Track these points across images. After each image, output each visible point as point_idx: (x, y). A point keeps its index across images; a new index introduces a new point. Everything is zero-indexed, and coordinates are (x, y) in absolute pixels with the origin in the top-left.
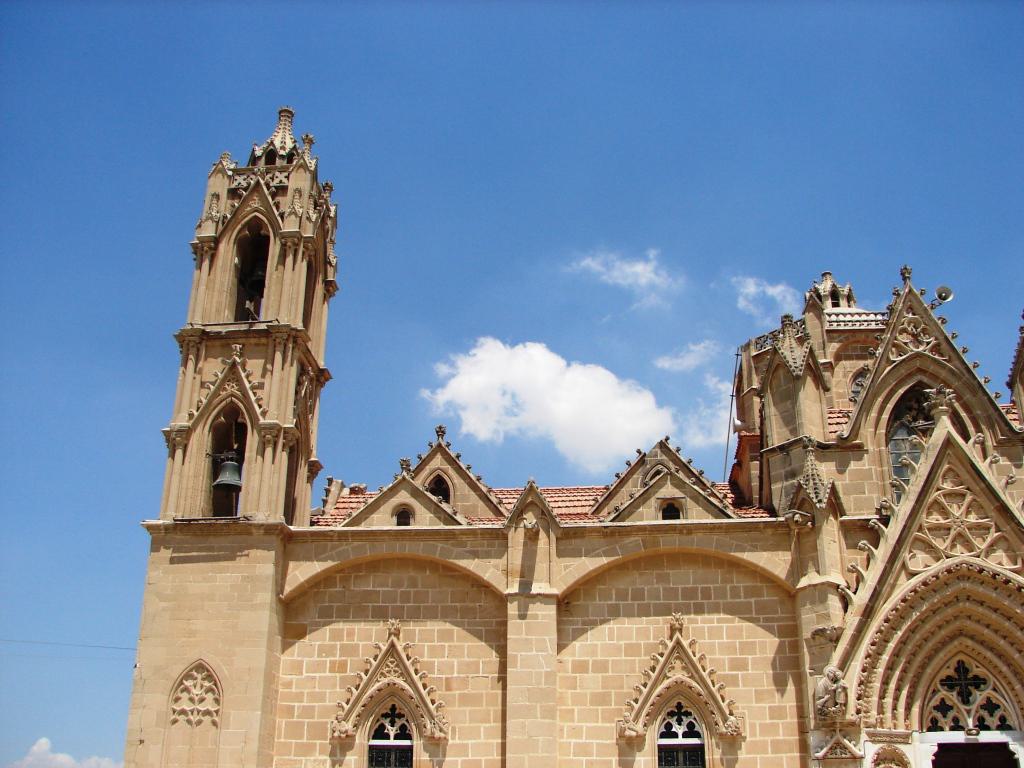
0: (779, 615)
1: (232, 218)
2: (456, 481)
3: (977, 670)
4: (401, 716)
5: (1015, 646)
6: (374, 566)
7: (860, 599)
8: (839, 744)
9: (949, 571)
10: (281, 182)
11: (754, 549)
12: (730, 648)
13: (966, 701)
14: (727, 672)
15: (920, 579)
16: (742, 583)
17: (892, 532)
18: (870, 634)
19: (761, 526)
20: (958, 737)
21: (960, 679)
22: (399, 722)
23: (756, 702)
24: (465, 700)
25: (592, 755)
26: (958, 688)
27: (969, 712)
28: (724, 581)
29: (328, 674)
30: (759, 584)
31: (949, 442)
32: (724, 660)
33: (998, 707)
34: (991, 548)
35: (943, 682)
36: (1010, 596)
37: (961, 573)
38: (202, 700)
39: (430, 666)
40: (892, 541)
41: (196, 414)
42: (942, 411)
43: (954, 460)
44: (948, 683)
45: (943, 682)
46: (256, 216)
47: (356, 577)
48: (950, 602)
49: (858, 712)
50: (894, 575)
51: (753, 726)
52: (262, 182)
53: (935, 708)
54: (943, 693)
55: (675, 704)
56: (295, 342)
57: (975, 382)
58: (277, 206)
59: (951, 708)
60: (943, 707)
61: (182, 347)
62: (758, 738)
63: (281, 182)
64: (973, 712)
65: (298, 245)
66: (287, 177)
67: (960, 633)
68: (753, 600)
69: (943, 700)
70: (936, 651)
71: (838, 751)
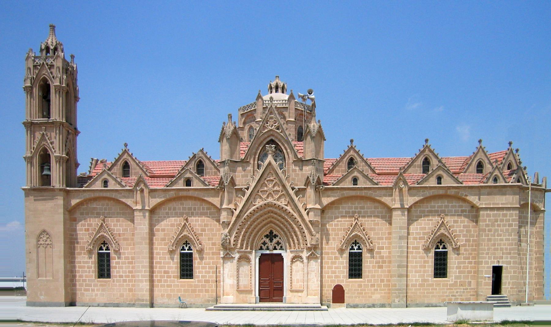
0: (216, 216)
1: (36, 78)
2: (131, 163)
4: (107, 244)
6: (95, 199)
7: (236, 213)
8: (228, 253)
9: (265, 205)
10: (52, 63)
11: (208, 196)
12: (201, 225)
16: (206, 206)
17: (248, 193)
18: (240, 223)
20: (268, 252)
22: (106, 246)
24: (125, 239)
25: (337, 238)
26: (273, 238)
27: (271, 245)
29: (84, 232)
31: (270, 164)
32: (199, 229)
35: (265, 236)
38: (46, 241)
39: (114, 230)
40: (248, 195)
41: (33, 151)
42: (270, 153)
43: (271, 169)
44: (267, 236)
45: (265, 236)
46: (44, 77)
47: (90, 203)
50: (248, 205)
51: (206, 248)
52: (45, 63)
53: (262, 243)
54: (265, 239)
55: (185, 241)
56: (63, 126)
58: (52, 73)
60: (264, 243)
61: (25, 127)
62: (208, 251)
63: (52, 63)
65: (60, 89)
66: (54, 60)
67: (271, 222)
68: (209, 211)
69: (265, 241)
70: (263, 227)
71: (228, 255)
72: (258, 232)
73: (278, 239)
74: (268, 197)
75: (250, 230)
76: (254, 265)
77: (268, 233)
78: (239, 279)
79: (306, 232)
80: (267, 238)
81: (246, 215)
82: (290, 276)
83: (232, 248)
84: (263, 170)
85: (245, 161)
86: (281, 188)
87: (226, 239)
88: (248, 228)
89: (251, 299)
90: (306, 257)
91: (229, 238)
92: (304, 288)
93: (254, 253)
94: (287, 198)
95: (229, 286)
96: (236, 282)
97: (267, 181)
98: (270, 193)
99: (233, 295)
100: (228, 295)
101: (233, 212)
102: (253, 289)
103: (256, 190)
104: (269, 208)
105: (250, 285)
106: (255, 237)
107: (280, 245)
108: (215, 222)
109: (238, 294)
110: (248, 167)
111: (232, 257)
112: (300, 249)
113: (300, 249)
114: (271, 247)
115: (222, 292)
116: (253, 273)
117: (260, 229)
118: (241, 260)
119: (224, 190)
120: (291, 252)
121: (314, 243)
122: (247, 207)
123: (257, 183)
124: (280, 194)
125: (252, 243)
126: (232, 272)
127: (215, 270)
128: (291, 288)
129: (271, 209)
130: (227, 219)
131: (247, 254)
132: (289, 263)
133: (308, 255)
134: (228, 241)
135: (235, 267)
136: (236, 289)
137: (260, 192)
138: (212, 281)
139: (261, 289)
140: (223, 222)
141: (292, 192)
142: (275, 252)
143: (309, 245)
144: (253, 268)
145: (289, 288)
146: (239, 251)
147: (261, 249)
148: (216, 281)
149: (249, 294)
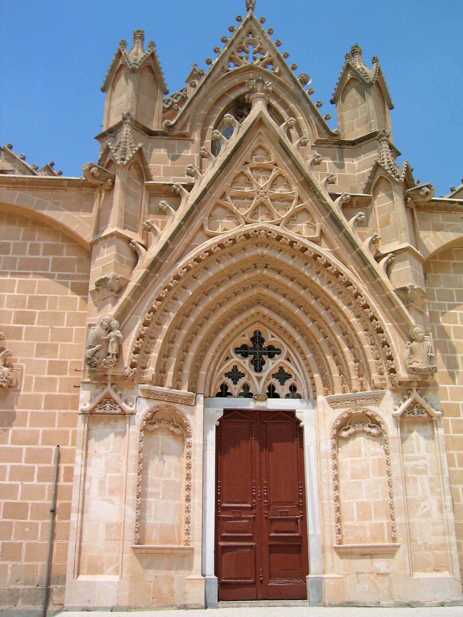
3: (270, 339)
5: (309, 315)
8: (108, 398)
9: (247, 236)
11: (55, 207)
12: (17, 302)
13: (258, 368)
14: (12, 325)
15: (217, 241)
19: (65, 183)
20: (250, 405)
21: (261, 354)
23: (37, 356)
27: (259, 379)
28: (25, 238)
30: (61, 243)
33: (290, 376)
34: (292, 218)
35: (237, 351)
36: (306, 264)
37: (259, 240)
44: (243, 351)
48: (248, 269)
49: (133, 365)
50: (191, 235)
51: (29, 379)
53: (226, 375)
54: (237, 359)
57: (300, 92)
59: (243, 375)
62: (33, 392)
64: (263, 380)
67: (258, 301)
68: (51, 257)
69: (235, 367)
70: (231, 317)
71: (108, 406)
72: (216, 331)
73: (279, 360)
74: (254, 214)
75: (192, 320)
76: (199, 450)
77: (246, 340)
78: (144, 502)
79: (387, 329)
80: (245, 355)
81: (181, 264)
82: (332, 493)
83: (125, 377)
84: (241, 135)
85: (176, 132)
86: (296, 190)
87: (108, 341)
88: (185, 314)
89: (188, 587)
90: (394, 417)
91: (118, 338)
92: (394, 539)
93: (200, 406)
94: (316, 220)
95: (102, 532)
96: (131, 513)
97: (252, 169)
98: (262, 204)
99: (116, 571)
100: (96, 570)
101: (136, 255)
102: (196, 545)
103: (218, 193)
104: (259, 251)
105: (184, 526)
106: (204, 349)
107: (289, 383)
108: (70, 294)
109: (139, 567)
110: (185, 151)
111: (124, 414)
112: (369, 391)
113: (369, 391)
114: (258, 388)
115: (71, 555)
116: (196, 481)
117: (224, 323)
118: (156, 426)
119: (113, 183)
120: (333, 403)
121: (420, 364)
122: (185, 240)
123: (222, 169)
124: (293, 207)
125: (196, 369)
126: (118, 471)
127: (53, 464)
128: (340, 542)
129: (265, 251)
130: (115, 271)
131: (178, 406)
132: (327, 444)
133: (400, 410)
134: (113, 349)
135: (134, 452)
136: (130, 543)
137: (229, 197)
138: (37, 510)
139: (223, 547)
140: (101, 283)
141: (335, 205)
142: (273, 404)
143: (403, 374)
144: (197, 461)
145: (331, 540)
146: (149, 391)
147: (224, 392)
148: (53, 511)
149: (180, 567)
